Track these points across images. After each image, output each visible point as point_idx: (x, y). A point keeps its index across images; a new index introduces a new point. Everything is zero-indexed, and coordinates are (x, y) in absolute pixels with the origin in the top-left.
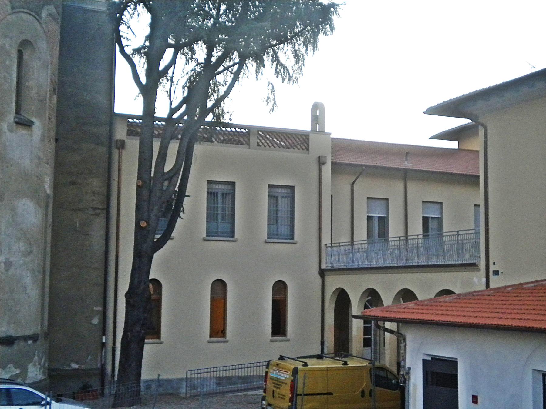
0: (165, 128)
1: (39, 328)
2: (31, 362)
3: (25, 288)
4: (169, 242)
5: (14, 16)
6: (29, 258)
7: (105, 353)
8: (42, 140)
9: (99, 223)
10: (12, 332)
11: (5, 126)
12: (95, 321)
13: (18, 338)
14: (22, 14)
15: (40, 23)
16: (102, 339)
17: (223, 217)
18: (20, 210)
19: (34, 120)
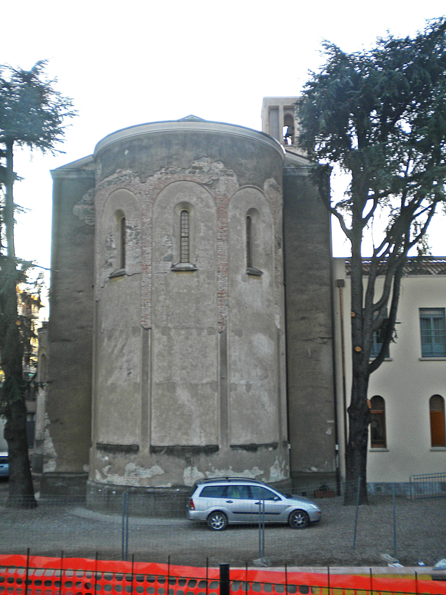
0: (371, 266)
1: (278, 437)
2: (273, 465)
3: (264, 405)
4: (384, 365)
5: (241, 191)
6: (266, 381)
7: (339, 459)
8: (271, 285)
9: (326, 351)
10: (256, 441)
11: (239, 278)
12: (329, 432)
13: (261, 445)
14: (248, 189)
15: (263, 193)
16: (335, 447)
17: (436, 340)
18: (255, 343)
19: (262, 270)
